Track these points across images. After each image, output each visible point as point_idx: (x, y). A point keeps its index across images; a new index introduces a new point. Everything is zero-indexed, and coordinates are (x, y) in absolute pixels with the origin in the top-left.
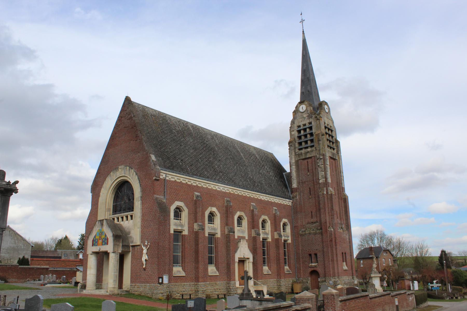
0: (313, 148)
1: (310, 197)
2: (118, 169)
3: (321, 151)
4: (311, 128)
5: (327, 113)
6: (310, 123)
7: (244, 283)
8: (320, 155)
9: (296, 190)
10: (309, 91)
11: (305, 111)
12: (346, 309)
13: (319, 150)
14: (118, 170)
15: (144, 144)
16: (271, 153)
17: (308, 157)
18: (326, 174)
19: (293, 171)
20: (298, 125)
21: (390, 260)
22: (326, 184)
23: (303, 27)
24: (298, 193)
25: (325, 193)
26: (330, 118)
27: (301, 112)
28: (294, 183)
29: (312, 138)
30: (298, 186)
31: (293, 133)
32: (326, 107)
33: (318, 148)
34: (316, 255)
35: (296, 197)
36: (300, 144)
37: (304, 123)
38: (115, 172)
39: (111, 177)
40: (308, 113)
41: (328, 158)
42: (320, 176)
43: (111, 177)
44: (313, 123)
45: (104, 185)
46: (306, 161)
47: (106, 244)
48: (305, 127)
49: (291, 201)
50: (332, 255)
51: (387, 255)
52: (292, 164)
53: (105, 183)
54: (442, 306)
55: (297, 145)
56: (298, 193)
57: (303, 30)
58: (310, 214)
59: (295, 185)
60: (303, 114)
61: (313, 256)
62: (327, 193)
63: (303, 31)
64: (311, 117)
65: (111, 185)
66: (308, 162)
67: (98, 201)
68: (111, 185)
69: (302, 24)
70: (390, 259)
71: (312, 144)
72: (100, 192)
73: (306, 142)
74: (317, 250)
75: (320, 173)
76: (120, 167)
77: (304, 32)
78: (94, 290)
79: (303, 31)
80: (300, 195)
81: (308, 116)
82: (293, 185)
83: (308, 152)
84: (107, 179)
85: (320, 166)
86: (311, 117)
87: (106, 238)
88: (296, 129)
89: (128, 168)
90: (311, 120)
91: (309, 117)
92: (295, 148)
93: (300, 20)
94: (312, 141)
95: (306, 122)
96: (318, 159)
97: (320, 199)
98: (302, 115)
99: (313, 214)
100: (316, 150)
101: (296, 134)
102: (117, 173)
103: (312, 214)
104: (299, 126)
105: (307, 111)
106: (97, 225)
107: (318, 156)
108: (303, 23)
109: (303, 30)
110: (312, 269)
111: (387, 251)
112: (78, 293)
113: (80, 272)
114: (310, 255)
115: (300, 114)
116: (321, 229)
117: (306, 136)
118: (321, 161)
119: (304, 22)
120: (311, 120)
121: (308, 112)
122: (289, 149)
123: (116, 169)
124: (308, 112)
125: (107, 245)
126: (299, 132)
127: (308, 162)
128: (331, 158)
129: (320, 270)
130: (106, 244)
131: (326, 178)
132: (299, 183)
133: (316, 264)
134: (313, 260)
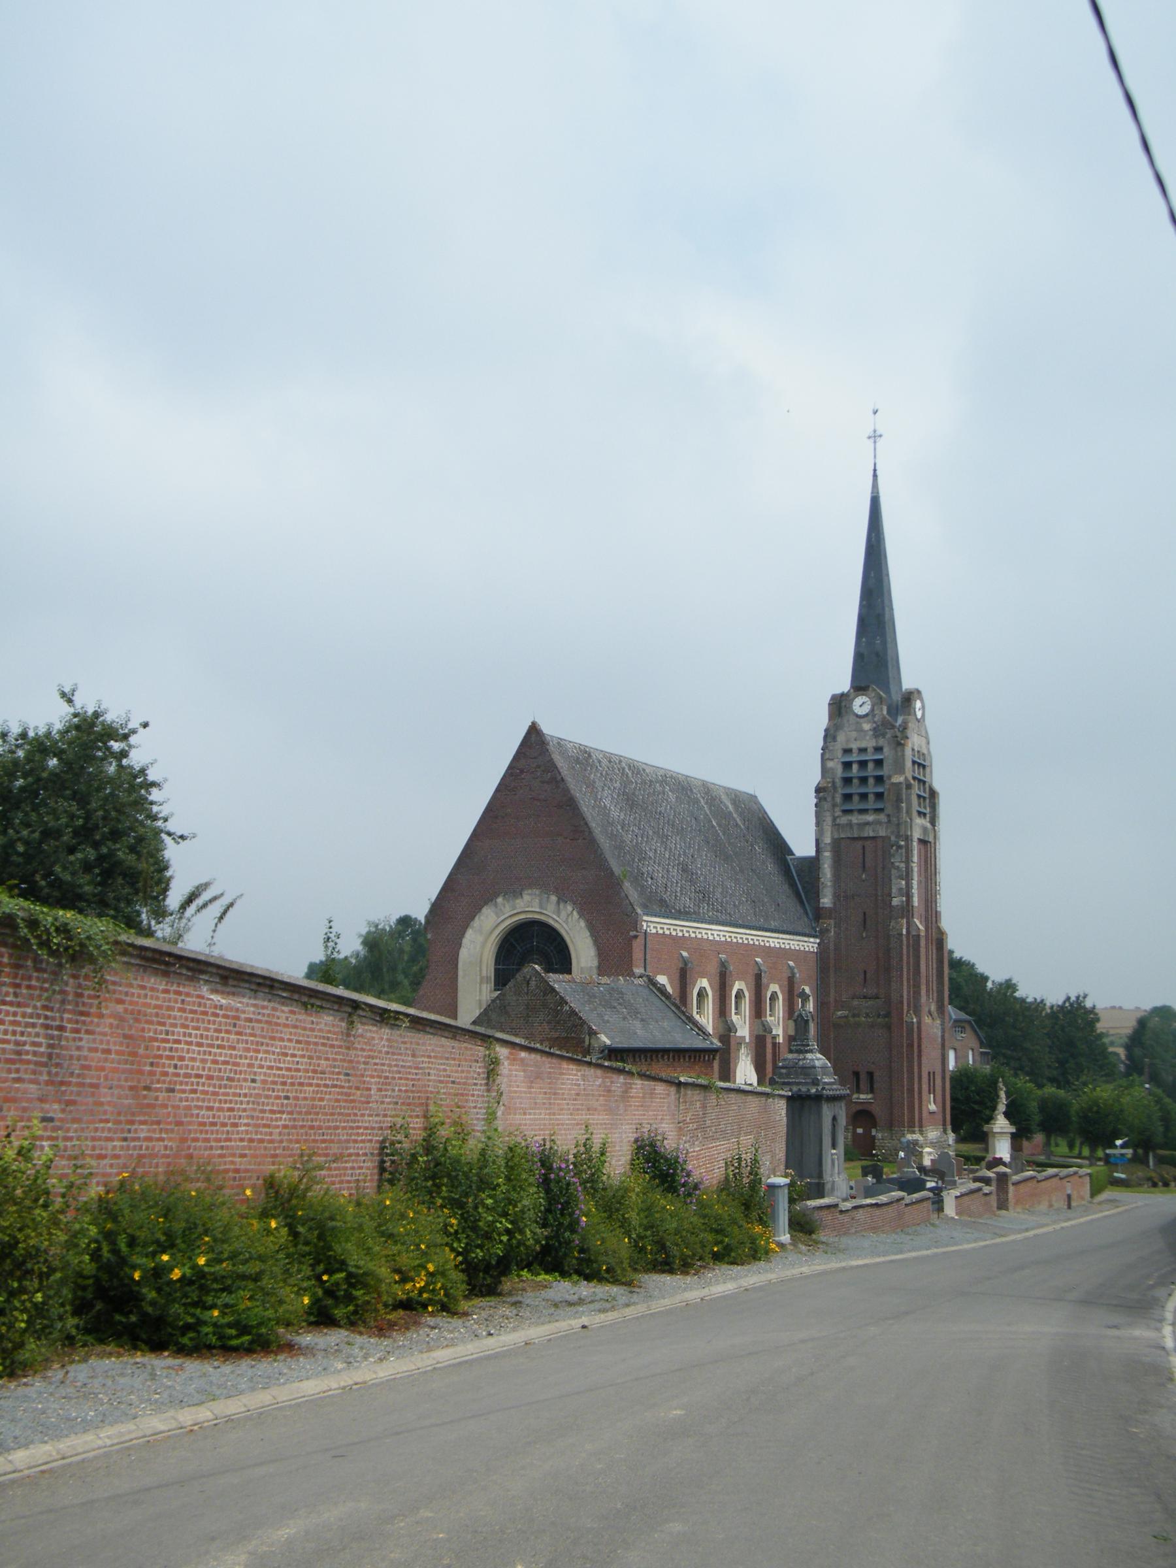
0: (882, 817)
1: (864, 935)
3: (902, 827)
4: (879, 763)
5: (918, 721)
6: (878, 749)
8: (898, 836)
9: (830, 913)
10: (877, 655)
11: (867, 715)
13: (898, 825)
16: (752, 793)
17: (866, 835)
18: (909, 886)
19: (826, 866)
20: (845, 747)
21: (970, 1053)
22: (907, 910)
23: (875, 457)
24: (832, 922)
25: (904, 932)
26: (923, 734)
27: (857, 716)
28: (825, 896)
29: (880, 790)
30: (835, 904)
31: (830, 764)
32: (918, 704)
33: (894, 820)
34: (871, 1075)
35: (828, 930)
36: (847, 797)
37: (863, 745)
40: (875, 722)
41: (915, 839)
42: (894, 890)
44: (886, 750)
45: (476, 923)
46: (860, 843)
48: (863, 757)
49: (818, 941)
50: (911, 1079)
51: (963, 1035)
52: (822, 845)
54: (205, 886)
55: (838, 799)
56: (832, 922)
57: (875, 465)
58: (862, 976)
59: (826, 901)
60: (862, 720)
61: (863, 1076)
62: (908, 932)
63: (875, 470)
64: (883, 735)
65: (497, 926)
66: (864, 847)
67: (457, 959)
69: (873, 445)
70: (973, 1050)
71: (879, 806)
73: (864, 796)
74: (873, 1063)
75: (894, 881)
77: (878, 473)
79: (875, 470)
80: (837, 925)
81: (875, 730)
82: (822, 901)
83: (868, 823)
85: (897, 864)
86: (883, 735)
88: (840, 756)
89: (554, 898)
90: (881, 742)
91: (877, 732)
92: (834, 805)
93: (870, 432)
94: (879, 796)
95: (869, 743)
96: (892, 846)
97: (891, 946)
98: (857, 723)
99: (868, 975)
100: (889, 821)
101: (839, 771)
102: (517, 901)
103: (865, 978)
104: (848, 751)
105: (874, 716)
106: (1039, 1172)
107: (893, 838)
108: (877, 444)
109: (875, 465)
110: (860, 1108)
111: (963, 1025)
114: (857, 1074)
115: (852, 719)
116: (888, 1015)
117: (864, 780)
118: (901, 854)
119: (880, 442)
120: (881, 742)
121: (876, 719)
122: (816, 805)
123: (518, 894)
124: (876, 719)
126: (847, 765)
127: (864, 847)
128: (921, 841)
129: (876, 1110)
131: (909, 896)
132: (836, 896)
133: (870, 1096)
134: (862, 1086)
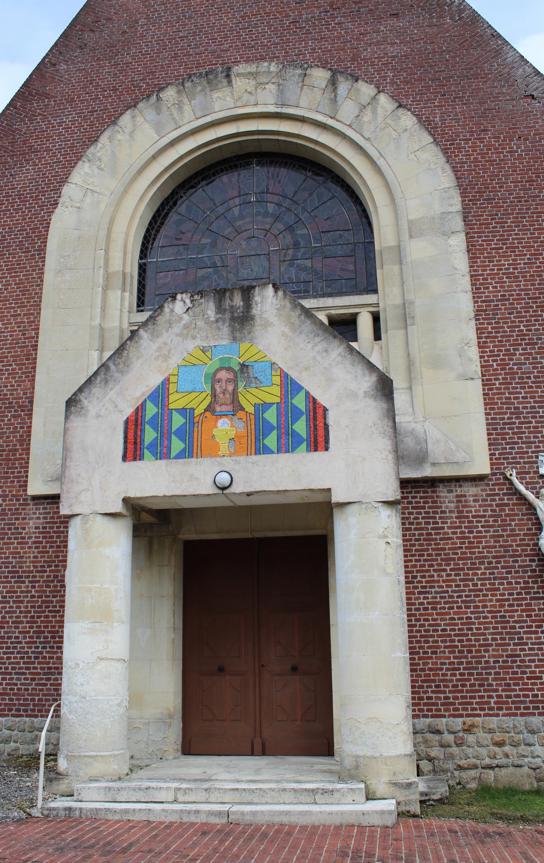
2: (228, 76)
7: (334, 772)
12: (143, 836)
14: (230, 82)
15: (222, 73)
38: (199, 88)
39: (159, 111)
43: (159, 111)
47: (304, 446)
53: (104, 139)
65: (154, 157)
68: (154, 157)
72: (64, 181)
76: (241, 68)
78: (153, 788)
84: (126, 119)
87: (300, 401)
102: (216, 95)
112: (35, 812)
113: (400, 617)
125: (319, 455)
130: (304, 446)
